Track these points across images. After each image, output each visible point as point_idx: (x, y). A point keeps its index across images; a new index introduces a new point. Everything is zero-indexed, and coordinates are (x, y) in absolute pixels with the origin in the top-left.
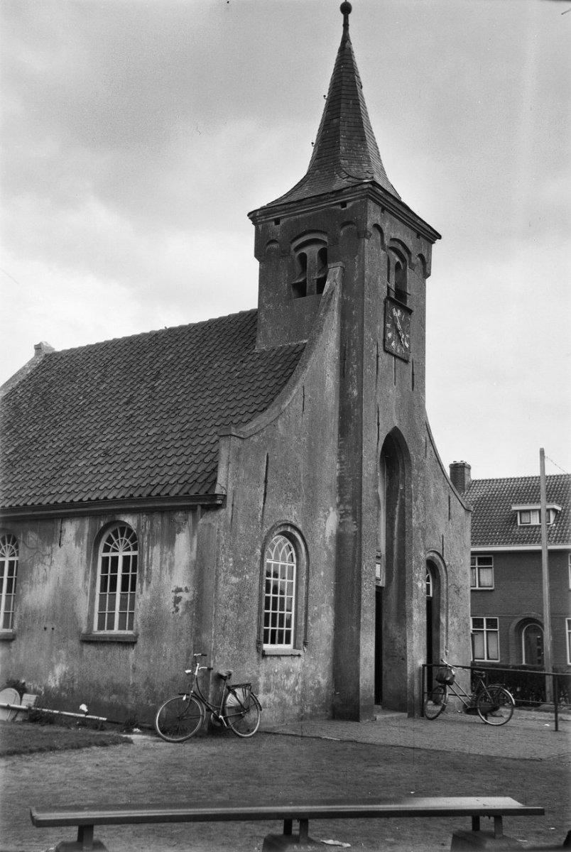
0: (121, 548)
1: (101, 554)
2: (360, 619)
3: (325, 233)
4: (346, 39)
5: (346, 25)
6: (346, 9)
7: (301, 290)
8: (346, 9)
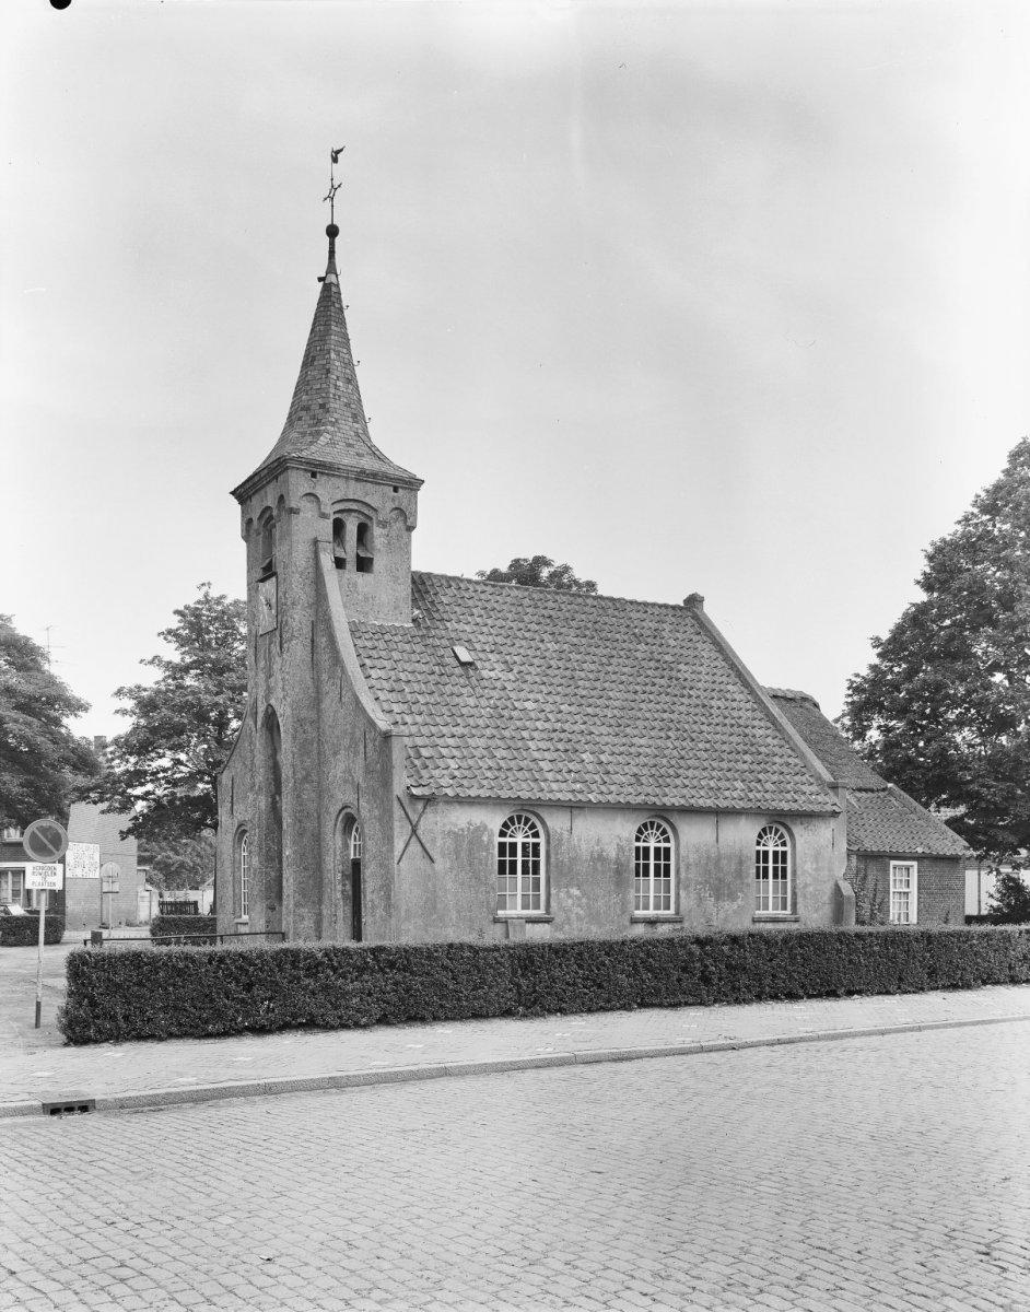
5: (332, 253)
6: (332, 232)
8: (332, 232)
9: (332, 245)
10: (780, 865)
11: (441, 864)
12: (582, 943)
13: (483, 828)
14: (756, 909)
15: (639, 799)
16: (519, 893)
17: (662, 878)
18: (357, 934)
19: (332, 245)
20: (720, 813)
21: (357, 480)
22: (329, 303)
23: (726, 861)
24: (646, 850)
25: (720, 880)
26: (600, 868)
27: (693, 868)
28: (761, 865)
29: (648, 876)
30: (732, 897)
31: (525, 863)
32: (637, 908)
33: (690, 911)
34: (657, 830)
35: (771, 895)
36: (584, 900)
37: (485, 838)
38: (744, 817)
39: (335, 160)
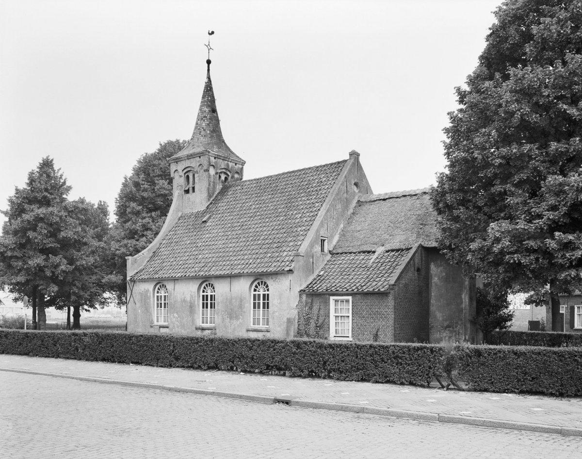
0: (261, 290)
1: (202, 294)
2: (477, 306)
3: (230, 172)
4: (209, 78)
5: (209, 70)
6: (209, 62)
7: (187, 192)
8: (209, 62)
11: (138, 305)
12: (142, 336)
13: (148, 291)
14: (246, 325)
15: (148, 276)
16: (163, 315)
17: (213, 309)
20: (231, 277)
21: (188, 159)
22: (209, 89)
23: (234, 300)
24: (259, 295)
25: (232, 310)
26: (184, 305)
27: (220, 304)
28: (213, 302)
29: (260, 308)
30: (237, 318)
31: (259, 299)
32: (203, 323)
33: (219, 325)
34: (264, 285)
35: (261, 317)
36: (179, 319)
37: (149, 295)
38: (242, 278)
39: (213, 33)
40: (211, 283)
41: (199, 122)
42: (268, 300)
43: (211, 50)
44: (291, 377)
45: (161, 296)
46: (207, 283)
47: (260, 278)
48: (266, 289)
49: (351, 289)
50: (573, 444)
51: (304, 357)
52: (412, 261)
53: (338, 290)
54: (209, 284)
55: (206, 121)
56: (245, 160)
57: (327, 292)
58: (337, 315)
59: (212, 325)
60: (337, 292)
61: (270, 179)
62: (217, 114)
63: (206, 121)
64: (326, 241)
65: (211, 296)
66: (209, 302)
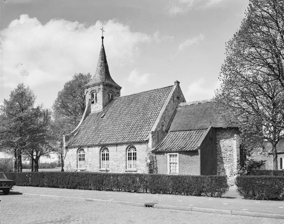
4: (103, 45)
5: (103, 42)
6: (103, 38)
8: (103, 38)
9: (103, 40)
10: (103, 157)
18: (176, 172)
19: (103, 40)
24: (131, 153)
28: (108, 157)
31: (131, 155)
34: (134, 148)
40: (106, 147)
41: (98, 68)
42: (108, 156)
43: (103, 32)
44: (163, 194)
45: (131, 153)
46: (104, 147)
47: (131, 145)
48: (134, 150)
49: (178, 149)
50: (282, 221)
51: (155, 184)
52: (208, 135)
53: (171, 150)
54: (106, 148)
55: (102, 67)
56: (121, 87)
57: (166, 151)
58: (170, 162)
59: (83, 168)
60: (171, 151)
61: (146, 93)
62: (107, 64)
63: (102, 67)
64: (164, 126)
65: (83, 155)
66: (105, 157)
